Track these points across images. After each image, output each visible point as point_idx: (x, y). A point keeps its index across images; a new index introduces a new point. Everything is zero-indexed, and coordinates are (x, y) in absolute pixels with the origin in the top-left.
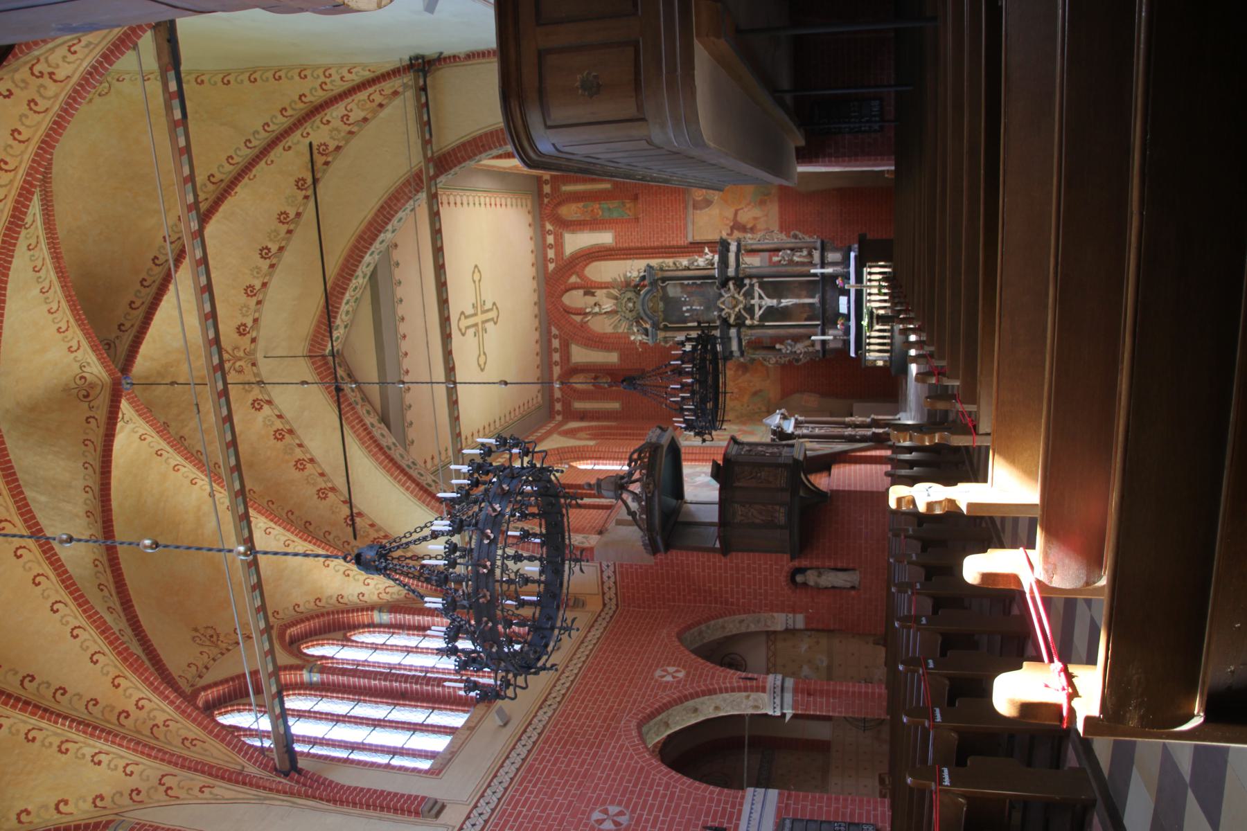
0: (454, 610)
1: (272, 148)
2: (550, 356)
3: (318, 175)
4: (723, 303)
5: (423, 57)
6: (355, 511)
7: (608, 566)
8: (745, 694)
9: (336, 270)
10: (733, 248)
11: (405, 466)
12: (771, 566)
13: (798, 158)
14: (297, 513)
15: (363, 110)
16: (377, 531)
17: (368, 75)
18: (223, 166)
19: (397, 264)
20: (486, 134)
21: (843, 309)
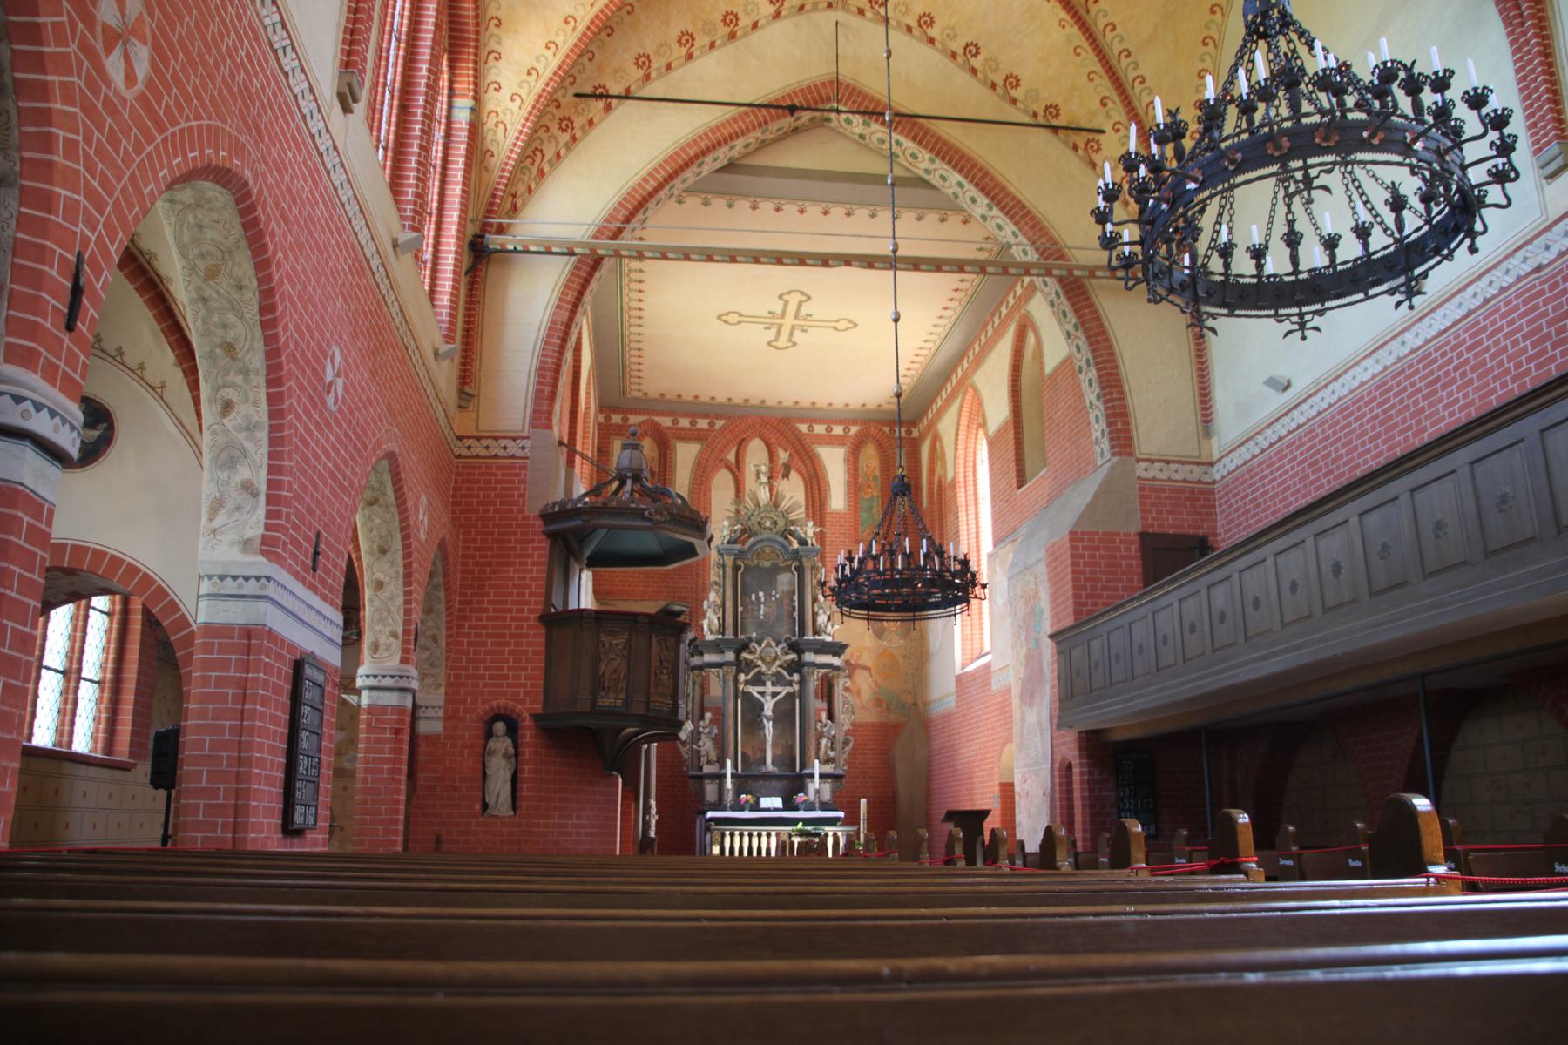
2: (685, 415)
4: (768, 645)
6: (614, 102)
7: (523, 448)
8: (400, 630)
9: (945, 136)
10: (836, 661)
12: (523, 685)
13: (1087, 732)
14: (627, 19)
16: (582, 128)
18: (1105, 16)
20: (1111, 347)
21: (765, 802)
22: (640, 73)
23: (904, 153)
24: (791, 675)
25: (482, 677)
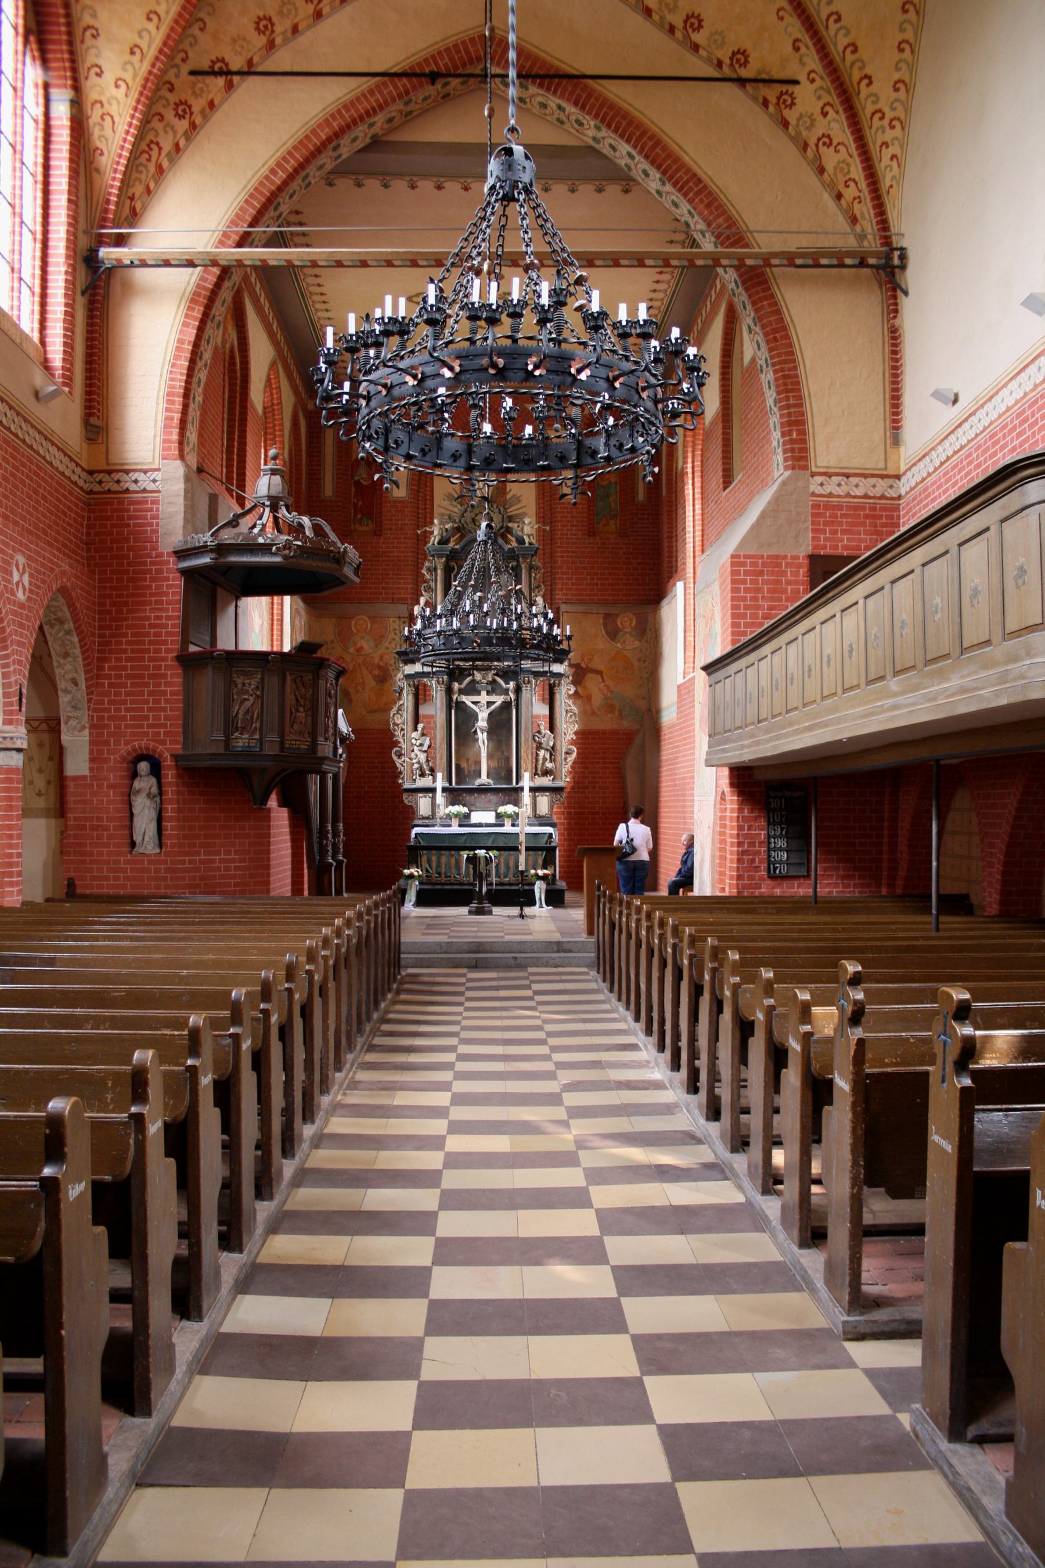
0: (469, 318)
1: (803, 23)
3: (749, 87)
5: (903, 267)
6: (236, 79)
7: (154, 481)
11: (307, 171)
12: (164, 726)
15: (835, 168)
17: (886, 182)
19: (600, 190)
20: (791, 345)
21: (476, 817)
22: (262, 40)
23: (568, 118)
24: (507, 683)
25: (124, 718)
